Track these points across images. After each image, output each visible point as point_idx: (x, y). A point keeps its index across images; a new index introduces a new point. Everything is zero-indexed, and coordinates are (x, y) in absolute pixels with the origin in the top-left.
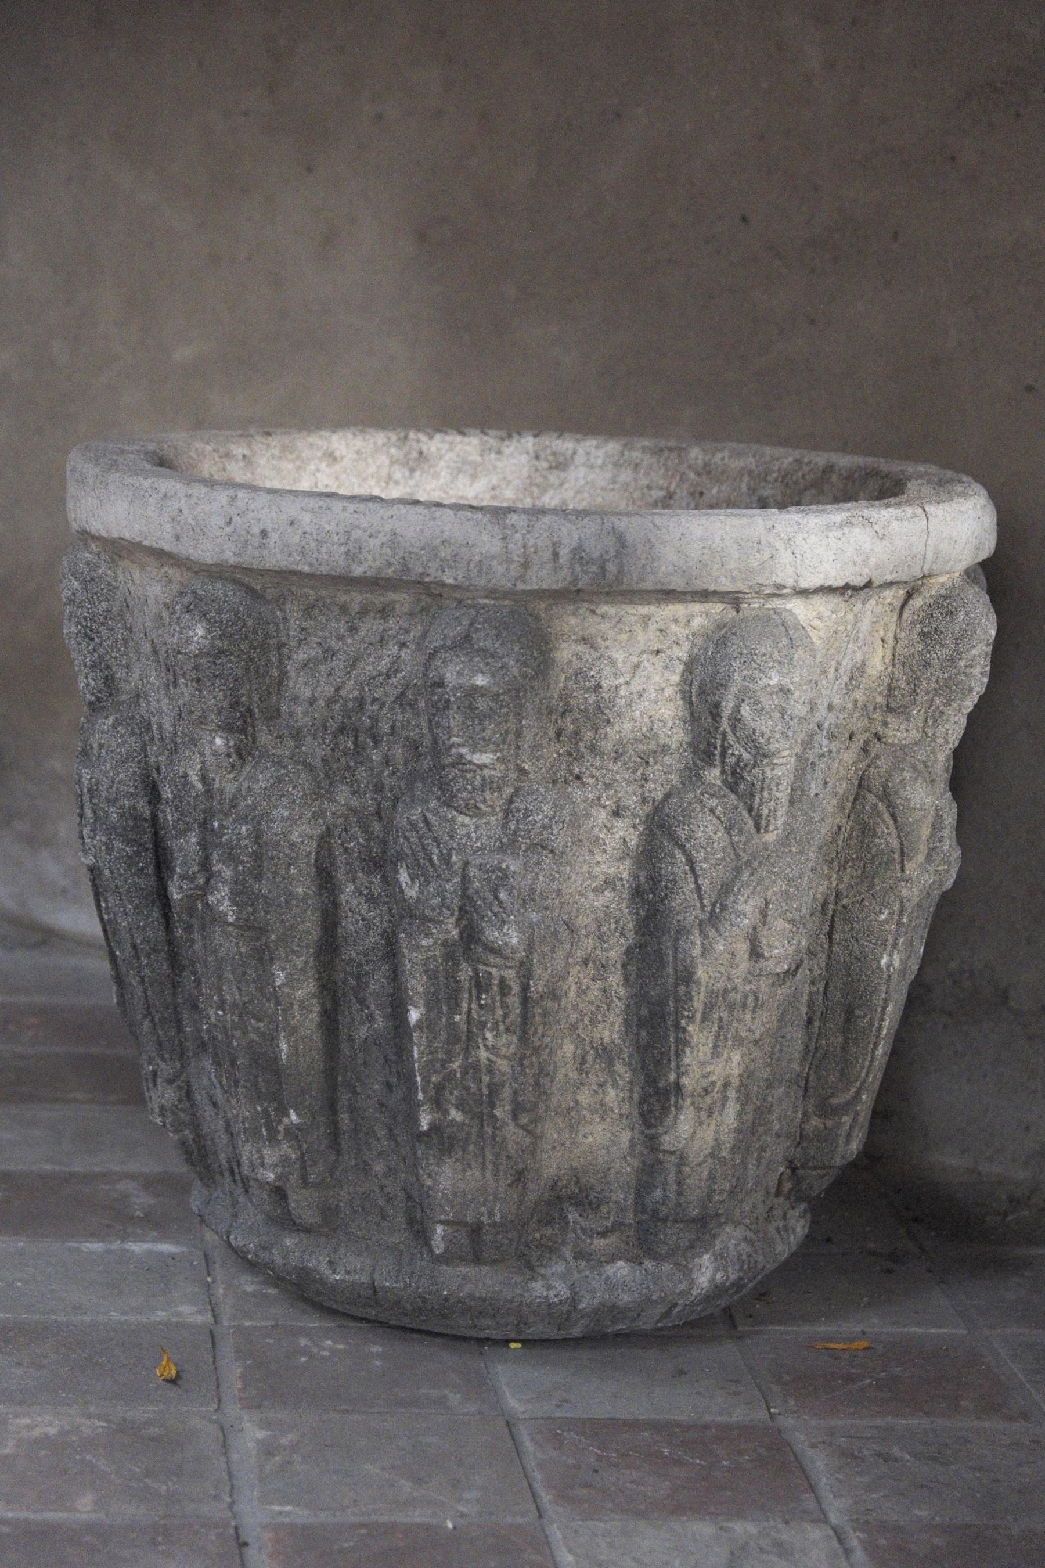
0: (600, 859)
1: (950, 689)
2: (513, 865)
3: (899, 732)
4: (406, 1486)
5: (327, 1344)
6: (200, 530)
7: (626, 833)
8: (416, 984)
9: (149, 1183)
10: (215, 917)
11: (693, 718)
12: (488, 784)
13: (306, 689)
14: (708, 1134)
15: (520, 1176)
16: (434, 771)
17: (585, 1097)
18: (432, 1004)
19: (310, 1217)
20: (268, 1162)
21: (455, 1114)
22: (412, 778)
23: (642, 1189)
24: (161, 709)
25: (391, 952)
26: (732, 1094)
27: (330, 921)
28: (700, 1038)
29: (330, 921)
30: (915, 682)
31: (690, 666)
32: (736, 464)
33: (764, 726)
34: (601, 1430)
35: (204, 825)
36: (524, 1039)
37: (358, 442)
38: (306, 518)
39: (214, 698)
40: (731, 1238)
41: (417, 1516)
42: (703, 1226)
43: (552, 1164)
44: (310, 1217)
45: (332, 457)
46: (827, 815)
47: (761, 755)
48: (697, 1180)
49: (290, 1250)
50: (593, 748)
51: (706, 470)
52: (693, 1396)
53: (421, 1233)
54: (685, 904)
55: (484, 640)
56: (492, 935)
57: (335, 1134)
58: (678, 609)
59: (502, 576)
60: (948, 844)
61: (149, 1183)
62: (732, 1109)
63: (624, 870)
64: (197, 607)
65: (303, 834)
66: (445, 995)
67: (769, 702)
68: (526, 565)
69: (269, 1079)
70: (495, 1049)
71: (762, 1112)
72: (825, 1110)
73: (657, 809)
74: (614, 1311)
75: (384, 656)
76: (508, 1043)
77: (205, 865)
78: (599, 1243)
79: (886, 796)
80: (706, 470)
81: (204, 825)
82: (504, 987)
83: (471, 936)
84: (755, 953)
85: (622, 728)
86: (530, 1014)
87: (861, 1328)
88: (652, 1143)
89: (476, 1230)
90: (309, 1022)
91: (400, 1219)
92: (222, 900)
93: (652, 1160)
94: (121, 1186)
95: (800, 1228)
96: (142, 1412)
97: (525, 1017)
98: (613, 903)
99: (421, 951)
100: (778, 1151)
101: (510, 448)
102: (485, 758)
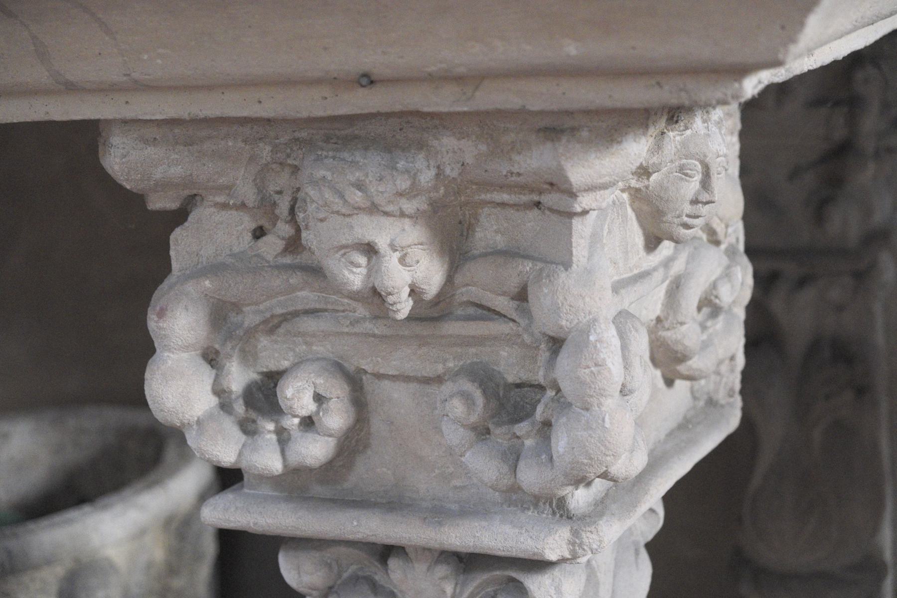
1: (198, 557)
3: (177, 583)
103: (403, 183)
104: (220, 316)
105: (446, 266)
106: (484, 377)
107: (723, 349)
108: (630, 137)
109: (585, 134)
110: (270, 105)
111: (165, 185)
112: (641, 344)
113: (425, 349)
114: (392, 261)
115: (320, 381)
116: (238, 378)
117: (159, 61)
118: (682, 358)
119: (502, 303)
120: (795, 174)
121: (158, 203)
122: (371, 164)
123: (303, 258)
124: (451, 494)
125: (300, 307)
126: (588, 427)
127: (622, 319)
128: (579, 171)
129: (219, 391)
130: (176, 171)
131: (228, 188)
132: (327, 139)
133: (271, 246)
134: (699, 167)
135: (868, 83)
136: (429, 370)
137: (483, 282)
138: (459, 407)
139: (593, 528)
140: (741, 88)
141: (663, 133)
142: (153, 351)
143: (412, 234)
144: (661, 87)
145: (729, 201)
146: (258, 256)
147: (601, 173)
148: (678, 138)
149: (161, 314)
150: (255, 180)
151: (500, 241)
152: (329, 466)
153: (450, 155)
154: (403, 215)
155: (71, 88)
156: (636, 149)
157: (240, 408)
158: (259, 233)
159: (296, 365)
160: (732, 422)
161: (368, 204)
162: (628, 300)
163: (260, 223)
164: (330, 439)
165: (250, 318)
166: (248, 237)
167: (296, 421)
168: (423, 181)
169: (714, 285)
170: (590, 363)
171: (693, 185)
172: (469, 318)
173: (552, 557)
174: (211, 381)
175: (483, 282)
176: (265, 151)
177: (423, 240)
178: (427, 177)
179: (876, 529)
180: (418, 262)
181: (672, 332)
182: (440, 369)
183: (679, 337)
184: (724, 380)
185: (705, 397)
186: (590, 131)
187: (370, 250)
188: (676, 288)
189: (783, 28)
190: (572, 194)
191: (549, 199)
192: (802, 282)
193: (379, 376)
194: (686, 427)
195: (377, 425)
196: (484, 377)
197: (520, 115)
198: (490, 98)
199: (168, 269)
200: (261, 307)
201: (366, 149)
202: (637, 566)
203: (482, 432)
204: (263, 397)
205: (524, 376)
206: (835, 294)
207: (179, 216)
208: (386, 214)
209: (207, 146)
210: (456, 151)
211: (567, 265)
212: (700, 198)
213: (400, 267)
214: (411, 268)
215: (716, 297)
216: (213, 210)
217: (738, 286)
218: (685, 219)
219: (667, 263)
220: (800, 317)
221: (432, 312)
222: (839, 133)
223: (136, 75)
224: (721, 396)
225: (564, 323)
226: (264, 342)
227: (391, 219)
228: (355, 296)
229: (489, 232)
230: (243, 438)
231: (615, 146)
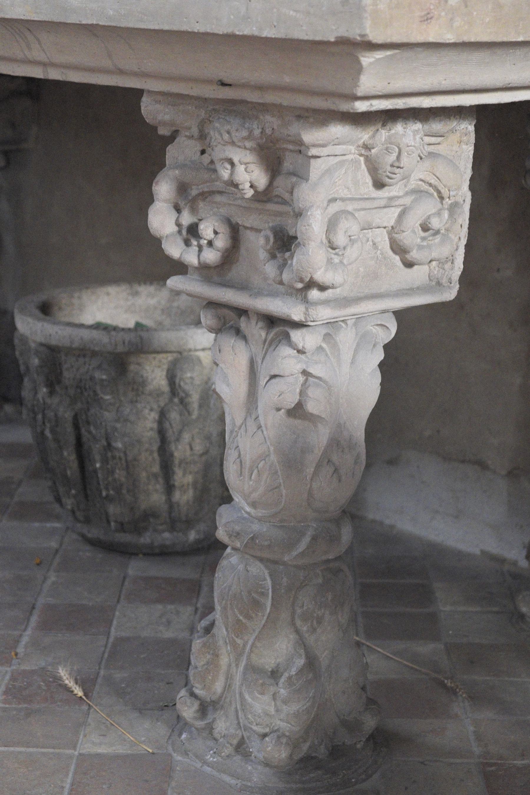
2: (118, 425)
7: (154, 415)
12: (111, 404)
15: (132, 509)
17: (150, 487)
21: (111, 492)
23: (170, 513)
26: (190, 487)
31: (168, 370)
36: (128, 473)
38: (60, 332)
44: (82, 519)
47: (187, 395)
50: (143, 393)
54: (170, 435)
56: (114, 444)
58: (164, 355)
59: (110, 348)
65: (69, 415)
66: (105, 461)
67: (188, 381)
68: (116, 345)
70: (120, 475)
76: (124, 473)
77: (44, 423)
78: (160, 527)
82: (120, 459)
84: (191, 449)
85: (150, 387)
86: (129, 466)
93: (171, 505)
98: (153, 434)
102: (107, 397)
103: (245, 133)
104: (182, 189)
105: (269, 176)
108: (332, 124)
109: (311, 120)
110: (196, 91)
111: (164, 124)
113: (261, 216)
114: (240, 169)
115: (216, 224)
117: (150, 64)
121: (163, 131)
122: (236, 122)
124: (266, 287)
125: (214, 189)
126: (303, 254)
129: (178, 224)
132: (224, 111)
134: (397, 150)
139: (314, 308)
140: (354, 105)
141: (378, 130)
142: (153, 201)
144: (327, 101)
146: (201, 163)
148: (387, 134)
149: (157, 183)
150: (198, 126)
153: (268, 123)
154: (245, 148)
157: (184, 232)
160: (450, 294)
161: (231, 141)
163: (204, 148)
164: (219, 253)
167: (206, 242)
168: (255, 134)
169: (429, 217)
170: (306, 224)
172: (277, 203)
174: (175, 219)
176: (203, 113)
177: (255, 161)
178: (257, 132)
180: (252, 171)
181: (399, 235)
183: (402, 238)
184: (447, 273)
185: (436, 280)
186: (314, 119)
189: (353, 79)
190: (308, 148)
193: (246, 228)
197: (290, 109)
200: (200, 187)
201: (236, 116)
202: (372, 352)
204: (193, 231)
207: (172, 138)
208: (239, 147)
209: (181, 108)
211: (307, 180)
212: (394, 164)
213: (245, 173)
215: (429, 223)
216: (185, 138)
218: (388, 174)
223: (143, 69)
225: (301, 205)
226: (201, 204)
227: (241, 149)
230: (185, 247)
231: (325, 128)
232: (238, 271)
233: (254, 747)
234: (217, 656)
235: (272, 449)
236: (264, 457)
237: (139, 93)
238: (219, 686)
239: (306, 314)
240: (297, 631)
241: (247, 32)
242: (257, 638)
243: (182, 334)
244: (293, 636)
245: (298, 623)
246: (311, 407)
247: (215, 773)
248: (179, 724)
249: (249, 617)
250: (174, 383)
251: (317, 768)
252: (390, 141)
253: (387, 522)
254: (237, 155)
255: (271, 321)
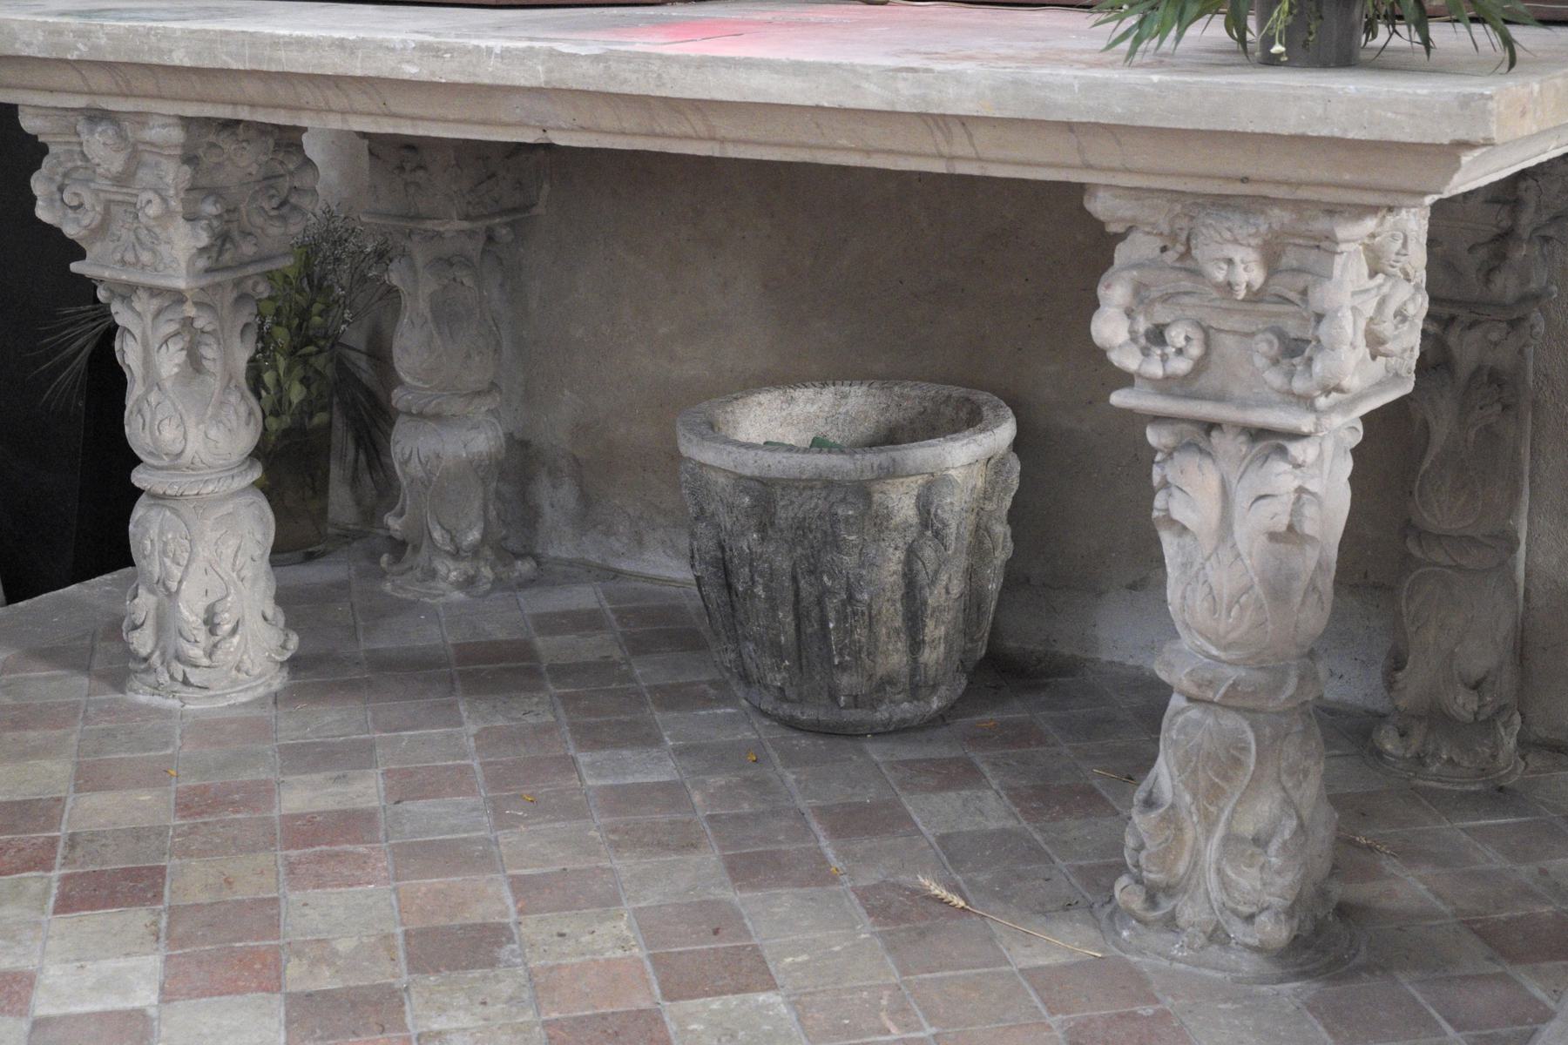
0: (892, 563)
1: (1006, 490)
3: (989, 506)
4: (849, 790)
5: (803, 742)
6: (744, 465)
8: (832, 615)
9: (712, 683)
10: (754, 596)
11: (920, 513)
12: (855, 546)
13: (784, 515)
14: (934, 656)
16: (836, 544)
18: (838, 621)
19: (794, 697)
20: (777, 679)
22: (825, 543)
23: (912, 676)
24: (727, 521)
25: (820, 602)
27: (797, 594)
28: (930, 624)
29: (797, 594)
30: (993, 488)
31: (918, 497)
32: (913, 394)
33: (946, 516)
34: (904, 763)
35: (751, 565)
37: (769, 396)
39: (753, 522)
40: (943, 690)
41: (857, 799)
42: (934, 688)
43: (880, 672)
45: (760, 404)
46: (967, 537)
47: (945, 525)
48: (931, 673)
49: (785, 709)
51: (902, 396)
52: (939, 749)
53: (834, 698)
54: (923, 578)
55: (850, 499)
56: (859, 597)
57: (801, 668)
59: (854, 476)
60: (1010, 544)
61: (712, 683)
62: (942, 646)
63: (900, 567)
64: (746, 491)
65: (787, 565)
66: (842, 618)
69: (778, 651)
70: (860, 634)
71: (951, 647)
72: (972, 640)
73: (911, 546)
74: (904, 720)
75: (815, 503)
76: (865, 632)
77: (752, 578)
78: (898, 697)
79: (987, 530)
80: (902, 396)
81: (751, 565)
83: (851, 597)
84: (948, 592)
87: (990, 717)
88: (915, 660)
89: (856, 697)
90: (791, 630)
91: (826, 695)
92: (759, 590)
94: (702, 686)
95: (964, 682)
96: (749, 773)
97: (870, 624)
99: (832, 604)
100: (956, 657)
101: (825, 391)
103: (1252, 230)
104: (1139, 290)
106: (1281, 335)
107: (1408, 342)
112: (1362, 325)
114: (1240, 268)
116: (1142, 325)
118: (1383, 343)
119: (1292, 295)
120: (1471, 249)
121: (1113, 228)
122: (1237, 219)
123: (1189, 264)
127: (1354, 309)
128: (1342, 231)
130: (1128, 214)
131: (1154, 225)
132: (1213, 204)
133: (1171, 256)
135: (1528, 191)
136: (1246, 329)
137: (1282, 285)
138: (1264, 346)
142: (1098, 306)
143: (1252, 256)
145: (1418, 257)
147: (1353, 234)
149: (1108, 287)
151: (1295, 264)
152: (1186, 377)
155: (1089, 167)
156: (1370, 224)
157: (1143, 341)
158: (1164, 249)
159: (1176, 321)
160: (1408, 387)
162: (1357, 301)
165: (1154, 293)
166: (1158, 251)
169: (1405, 303)
171: (1398, 245)
173: (1305, 429)
175: (1282, 285)
176: (1178, 208)
178: (1264, 228)
179: (1512, 510)
182: (1254, 328)
187: (1230, 262)
188: (1382, 303)
191: (1324, 244)
192: (1471, 326)
193: (1219, 331)
194: (1380, 385)
195: (1214, 357)
196: (1281, 335)
198: (1303, 194)
199: (1112, 263)
203: (1275, 362)
204: (1157, 336)
205: (1300, 335)
206: (1494, 336)
207: (1120, 237)
210: (1280, 217)
211: (1330, 277)
214: (1249, 273)
217: (1419, 306)
219: (1379, 287)
220: (1468, 349)
221: (1255, 297)
222: (1506, 223)
224: (1403, 372)
226: (1158, 307)
228: (1217, 286)
229: (1290, 259)
232: (1207, 382)
233: (1237, 930)
234: (1181, 830)
235: (1256, 579)
236: (1248, 589)
237: (1082, 187)
238: (1181, 867)
239: (1317, 424)
240: (1284, 789)
241: (1325, 132)
242: (1239, 802)
243: (938, 450)
244: (1279, 795)
245: (1284, 778)
246: (1309, 528)
247: (1191, 969)
248: (1119, 915)
249: (1226, 778)
250: (929, 512)
251: (1307, 948)
252: (1395, 226)
253: (1131, 662)
254: (1238, 254)
255: (1258, 434)
